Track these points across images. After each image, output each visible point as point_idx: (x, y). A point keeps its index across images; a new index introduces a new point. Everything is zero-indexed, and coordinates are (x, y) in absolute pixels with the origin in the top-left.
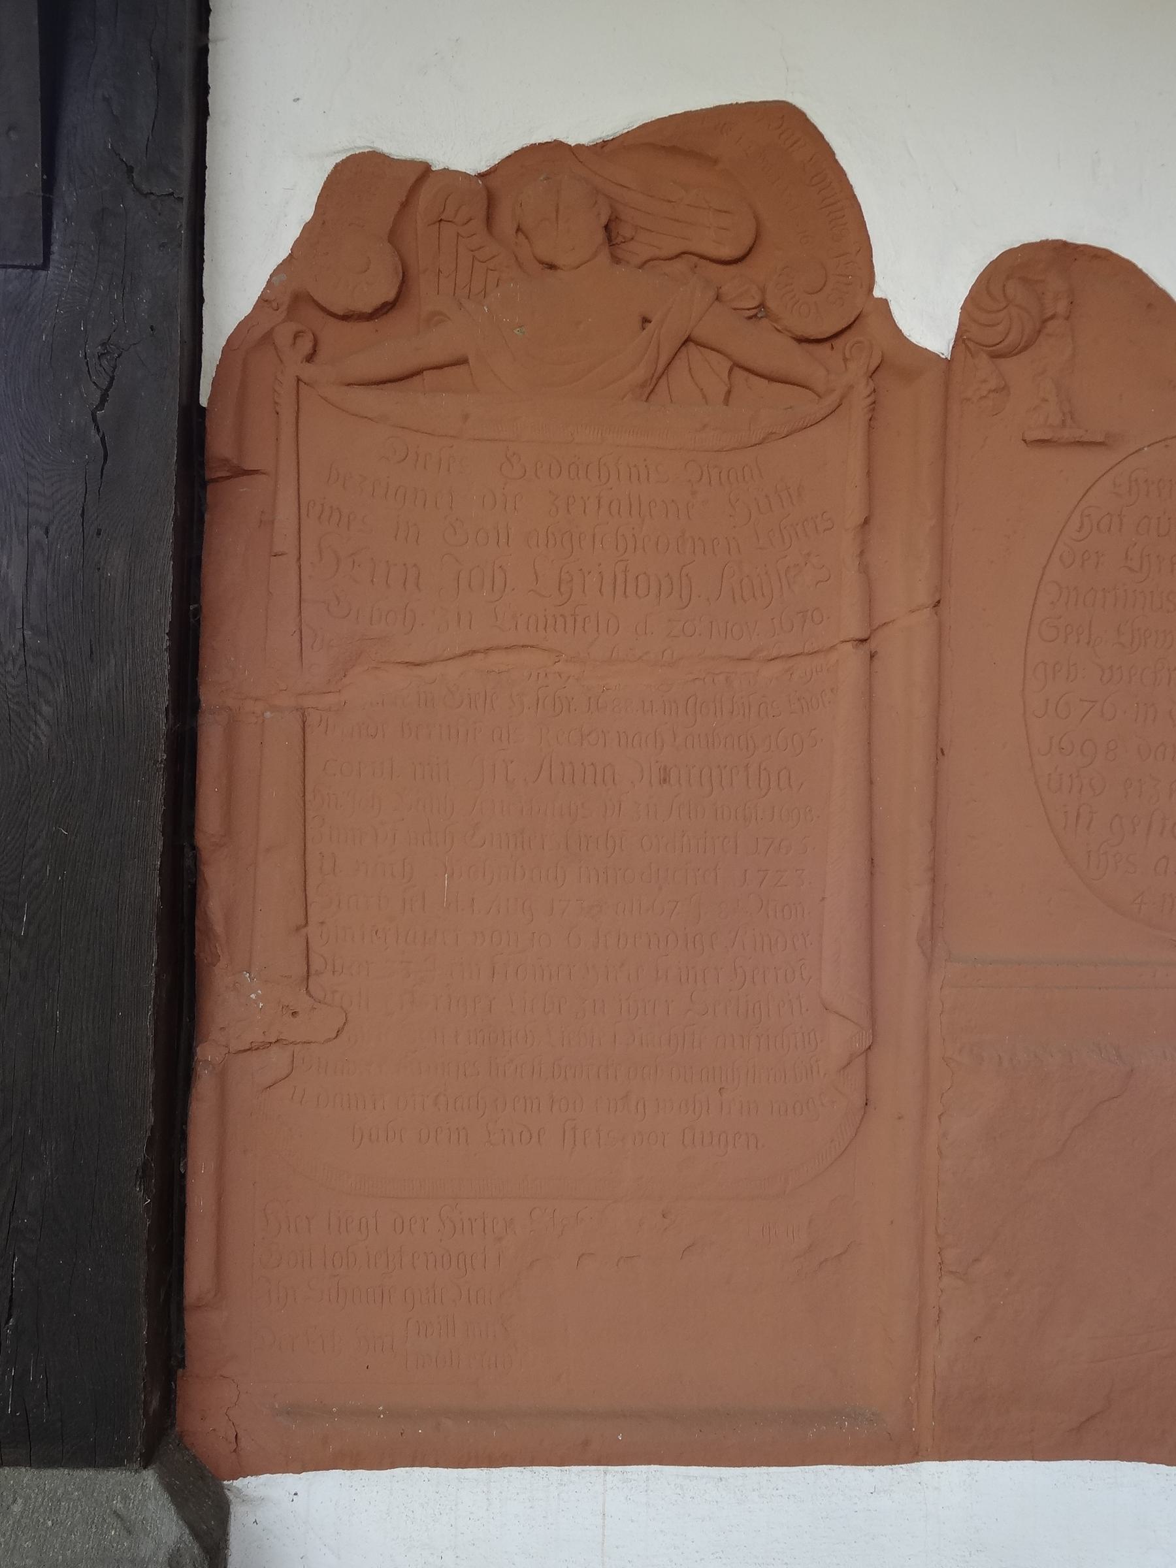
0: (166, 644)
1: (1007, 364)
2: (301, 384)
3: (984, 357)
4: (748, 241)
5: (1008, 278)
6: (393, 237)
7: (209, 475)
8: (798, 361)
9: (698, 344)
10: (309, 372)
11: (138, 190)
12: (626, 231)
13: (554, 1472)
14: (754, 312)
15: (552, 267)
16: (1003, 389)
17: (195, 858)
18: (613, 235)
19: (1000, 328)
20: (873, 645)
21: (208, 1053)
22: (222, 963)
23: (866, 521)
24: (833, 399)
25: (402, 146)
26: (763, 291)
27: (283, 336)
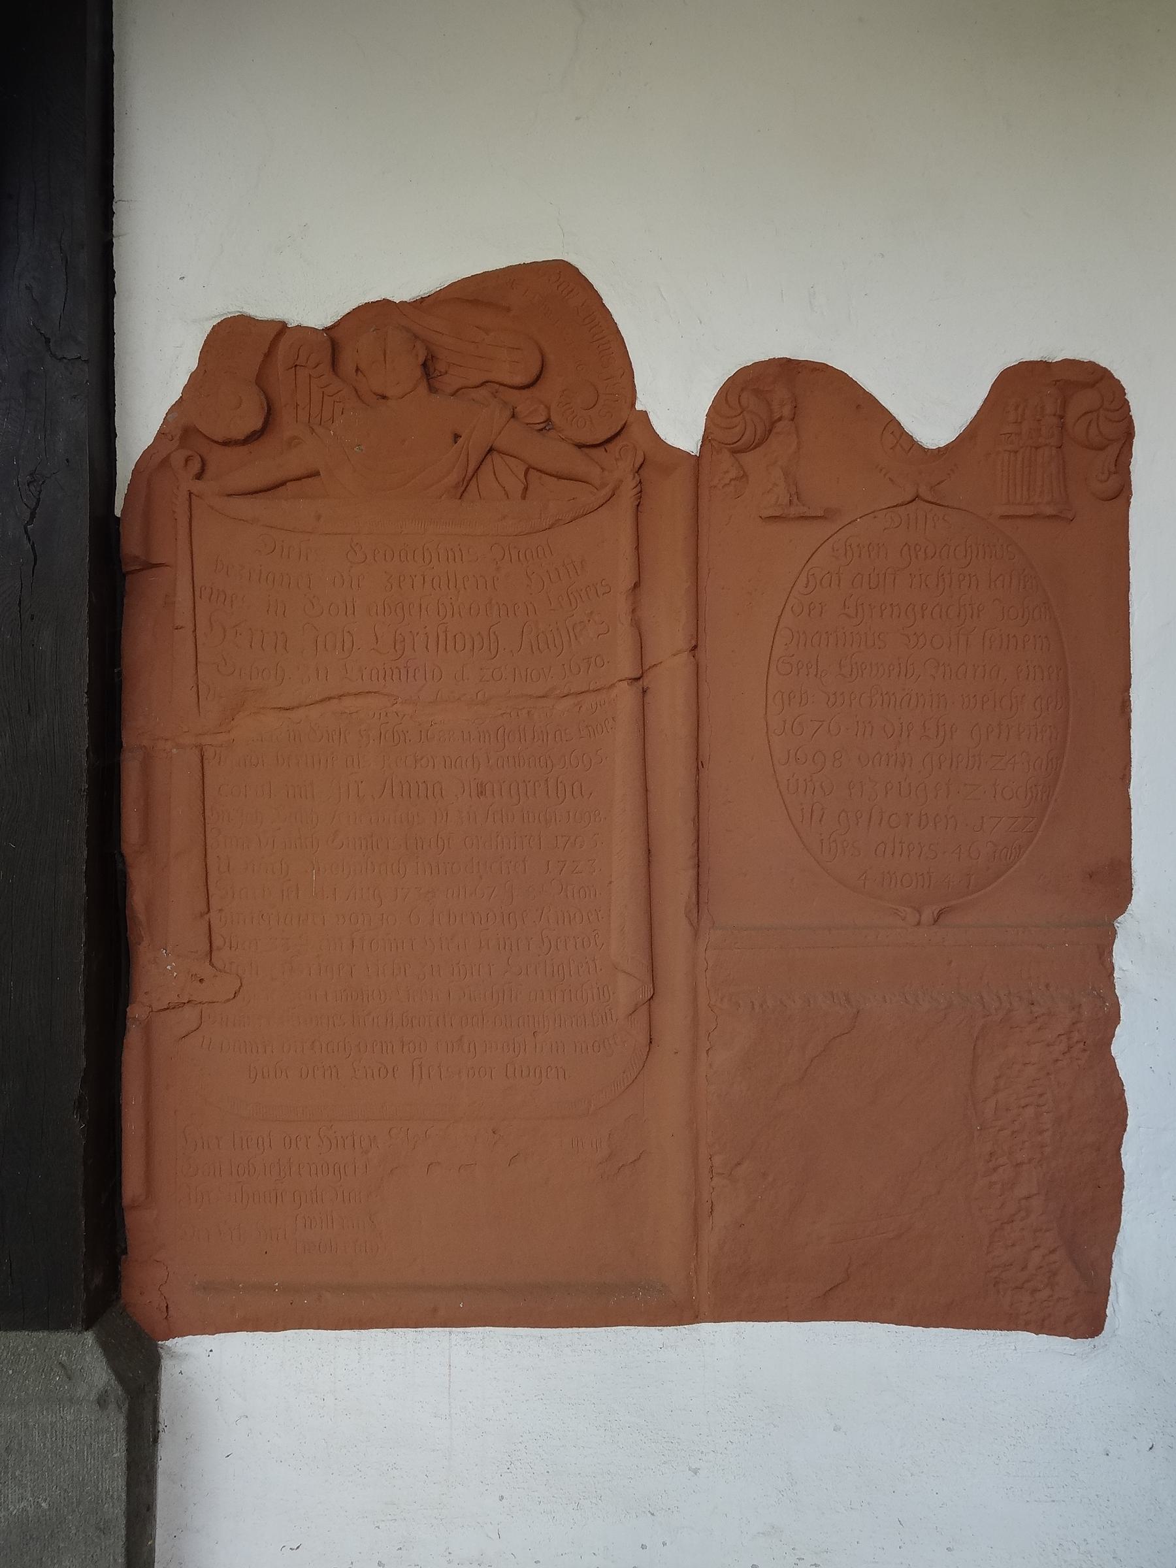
0: (85, 700)
1: (747, 458)
2: (193, 497)
3: (726, 455)
4: (535, 371)
5: (742, 390)
6: (260, 380)
7: (125, 569)
8: (580, 464)
9: (499, 452)
10: (198, 486)
11: (53, 355)
12: (441, 366)
13: (410, 1332)
14: (542, 426)
15: (384, 397)
16: (744, 476)
17: (124, 862)
18: (432, 370)
19: (737, 429)
20: (645, 682)
21: (136, 1012)
22: (145, 943)
23: (637, 585)
24: (606, 491)
25: (262, 311)
26: (548, 408)
27: (178, 458)
